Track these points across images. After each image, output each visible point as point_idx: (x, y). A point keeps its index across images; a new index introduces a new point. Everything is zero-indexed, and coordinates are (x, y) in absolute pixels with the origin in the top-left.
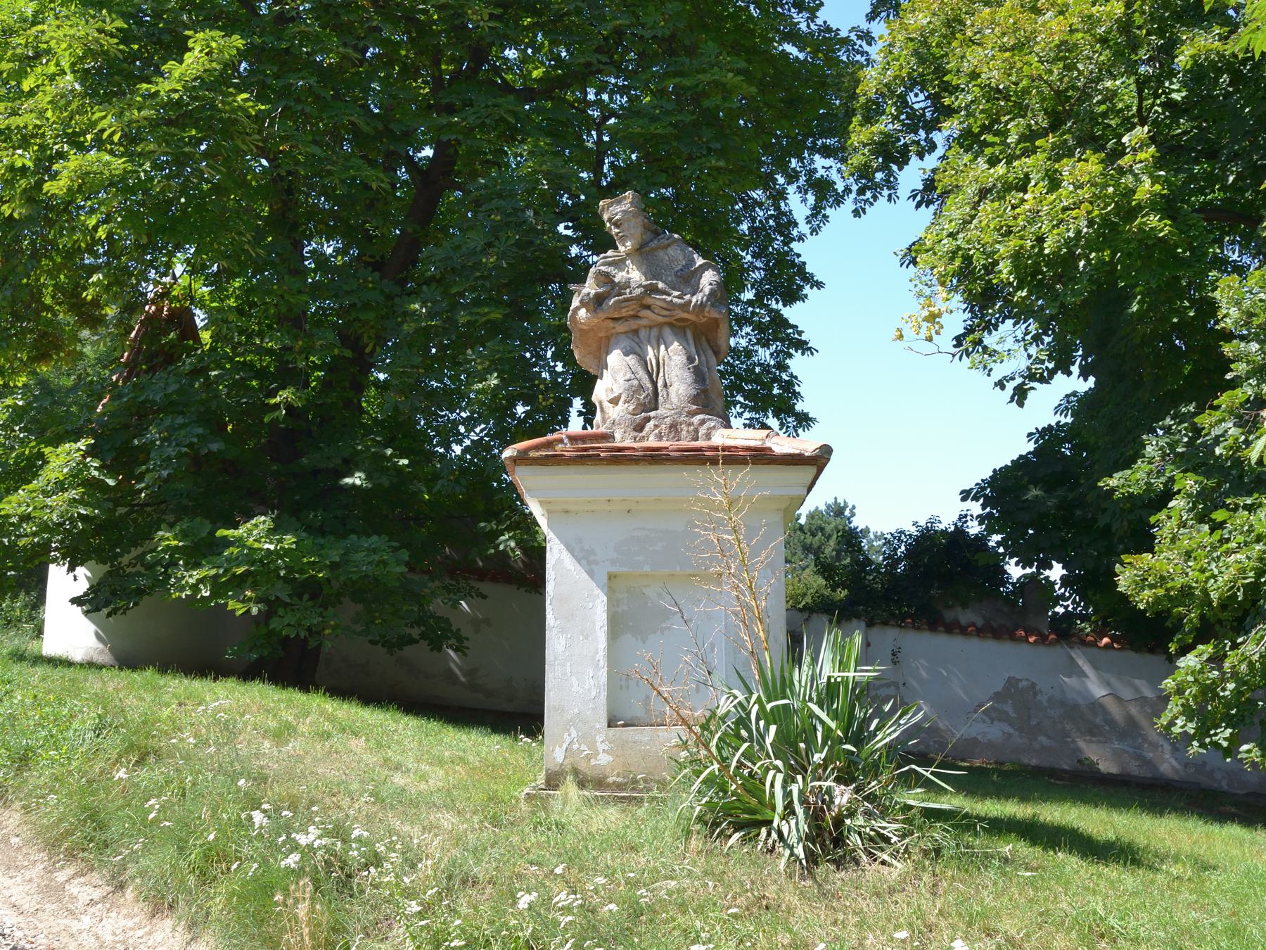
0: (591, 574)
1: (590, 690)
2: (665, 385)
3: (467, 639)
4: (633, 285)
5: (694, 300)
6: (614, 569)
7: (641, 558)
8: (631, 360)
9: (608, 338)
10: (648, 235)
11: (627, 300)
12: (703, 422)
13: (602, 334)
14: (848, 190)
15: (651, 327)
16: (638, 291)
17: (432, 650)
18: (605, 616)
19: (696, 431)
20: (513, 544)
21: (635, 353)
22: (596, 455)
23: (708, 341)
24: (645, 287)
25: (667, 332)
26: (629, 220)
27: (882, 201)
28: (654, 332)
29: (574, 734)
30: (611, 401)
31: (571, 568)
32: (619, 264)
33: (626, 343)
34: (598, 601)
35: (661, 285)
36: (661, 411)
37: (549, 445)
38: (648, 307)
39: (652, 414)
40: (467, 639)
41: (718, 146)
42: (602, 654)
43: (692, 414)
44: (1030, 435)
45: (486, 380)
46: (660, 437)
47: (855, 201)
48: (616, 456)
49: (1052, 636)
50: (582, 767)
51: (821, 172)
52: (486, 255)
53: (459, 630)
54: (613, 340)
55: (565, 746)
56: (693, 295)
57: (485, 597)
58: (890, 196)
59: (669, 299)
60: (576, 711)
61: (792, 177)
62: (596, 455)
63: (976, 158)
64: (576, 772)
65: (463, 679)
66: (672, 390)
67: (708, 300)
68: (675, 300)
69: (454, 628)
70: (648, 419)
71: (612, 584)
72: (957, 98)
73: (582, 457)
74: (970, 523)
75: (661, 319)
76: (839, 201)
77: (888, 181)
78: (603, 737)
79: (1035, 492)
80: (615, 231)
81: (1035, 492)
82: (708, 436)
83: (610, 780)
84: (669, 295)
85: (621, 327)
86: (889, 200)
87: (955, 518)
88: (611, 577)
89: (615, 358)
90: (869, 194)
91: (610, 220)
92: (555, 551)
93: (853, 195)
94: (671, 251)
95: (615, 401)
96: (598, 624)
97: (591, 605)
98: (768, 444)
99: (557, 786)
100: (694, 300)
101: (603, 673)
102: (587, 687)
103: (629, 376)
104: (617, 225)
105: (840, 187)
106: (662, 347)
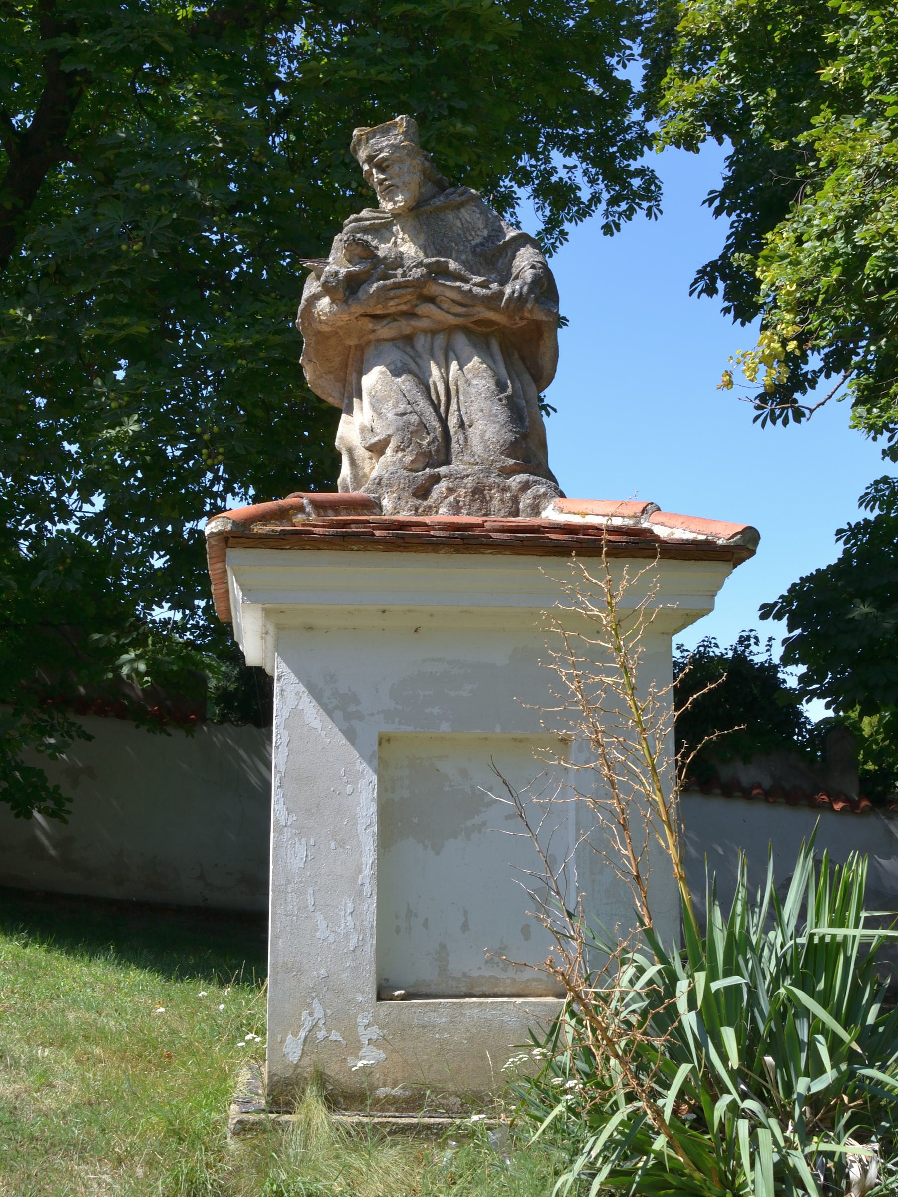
0: (351, 735)
1: (347, 935)
2: (462, 425)
3: (70, 800)
4: (408, 263)
5: (508, 290)
6: (389, 728)
7: (436, 710)
8: (404, 382)
9: (361, 349)
10: (429, 188)
11: (397, 286)
12: (526, 486)
13: (352, 342)
14: (595, 199)
15: (433, 333)
16: (417, 273)
17: (17, 816)
18: (373, 808)
19: (515, 500)
20: (142, 667)
21: (410, 372)
22: (358, 533)
23: (523, 359)
24: (427, 266)
25: (461, 341)
26: (401, 161)
27: (640, 214)
28: (440, 340)
29: (319, 1013)
30: (369, 449)
31: (316, 724)
32: (382, 230)
33: (396, 355)
34: (362, 783)
35: (453, 265)
36: (457, 466)
37: (283, 514)
38: (432, 300)
39: (443, 470)
40: (70, 800)
41: (464, 105)
42: (368, 871)
43: (508, 472)
44: (839, 532)
45: (121, 424)
46: (456, 508)
47: (606, 214)
48: (402, 537)
49: (864, 803)
50: (333, 1069)
51: (562, 173)
52: (130, 240)
53: (57, 787)
54: (370, 352)
55: (303, 1034)
56: (503, 283)
57: (89, 738)
58: (649, 209)
59: (466, 287)
60: (323, 971)
61: (523, 177)
62: (358, 533)
63: (869, 123)
64: (321, 1079)
65: (53, 852)
66: (474, 434)
67: (531, 291)
68: (477, 290)
69: (50, 784)
70: (437, 479)
71: (384, 753)
72: (846, 34)
73: (344, 536)
74: (753, 648)
75: (452, 320)
76: (584, 213)
77: (647, 189)
78: (369, 1020)
79: (862, 609)
80: (377, 176)
81: (862, 609)
82: (536, 510)
83: (382, 1092)
84: (466, 281)
85: (385, 331)
86: (649, 215)
87: (734, 641)
88: (384, 740)
89: (373, 379)
90: (624, 206)
91: (370, 159)
92: (290, 696)
93: (602, 206)
94: (465, 214)
95: (377, 449)
96: (362, 822)
97: (349, 788)
98: (645, 525)
99: (289, 1103)
100: (508, 290)
101: (371, 906)
102: (341, 930)
103: (402, 407)
104: (381, 168)
105: (585, 194)
106: (454, 366)
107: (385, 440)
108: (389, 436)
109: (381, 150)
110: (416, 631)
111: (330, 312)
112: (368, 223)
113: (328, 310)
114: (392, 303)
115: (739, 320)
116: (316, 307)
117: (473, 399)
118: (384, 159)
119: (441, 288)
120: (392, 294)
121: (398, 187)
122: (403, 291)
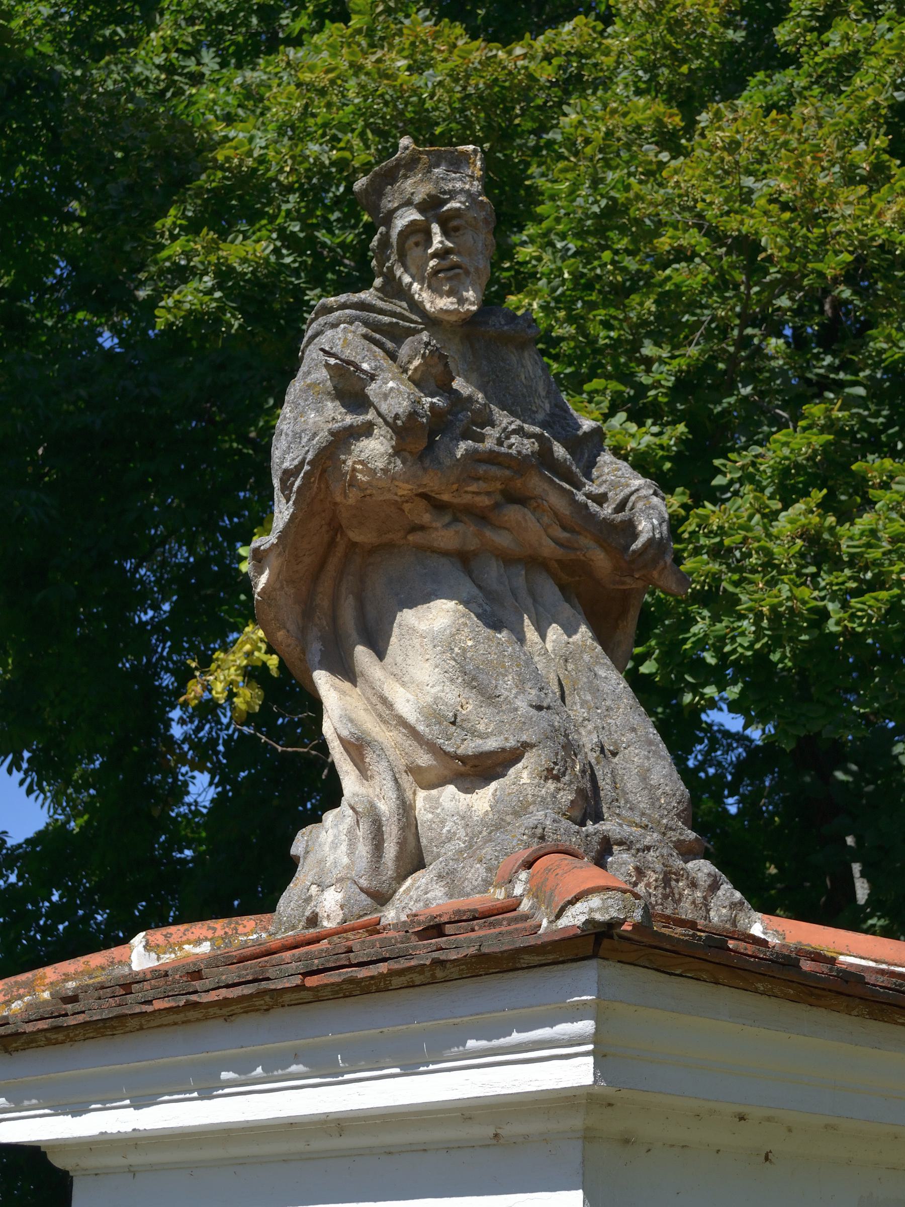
25: (549, 591)
85: (446, 536)
107: (513, 750)
108: (526, 746)
109: (453, 194)
110: (767, 1158)
111: (385, 471)
112: (387, 319)
113: (380, 465)
114: (473, 488)
115: (362, 654)
116: (349, 452)
117: (608, 703)
118: (456, 212)
119: (546, 486)
120: (482, 469)
121: (467, 273)
122: (494, 470)
